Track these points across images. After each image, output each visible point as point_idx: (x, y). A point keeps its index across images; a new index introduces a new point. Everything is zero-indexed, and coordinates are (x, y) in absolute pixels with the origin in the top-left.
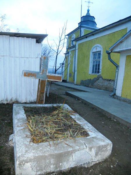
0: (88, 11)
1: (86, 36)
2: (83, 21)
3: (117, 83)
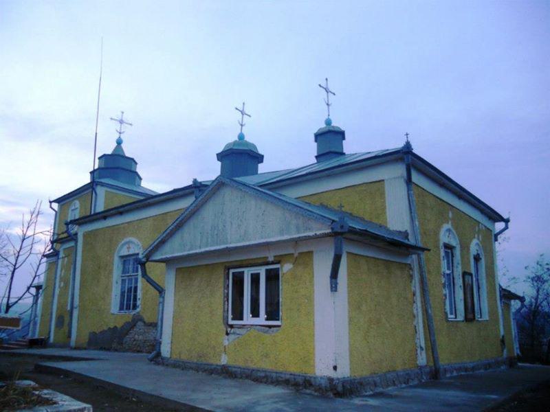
0: (119, 142)
1: (104, 216)
2: (103, 166)
3: (162, 327)
